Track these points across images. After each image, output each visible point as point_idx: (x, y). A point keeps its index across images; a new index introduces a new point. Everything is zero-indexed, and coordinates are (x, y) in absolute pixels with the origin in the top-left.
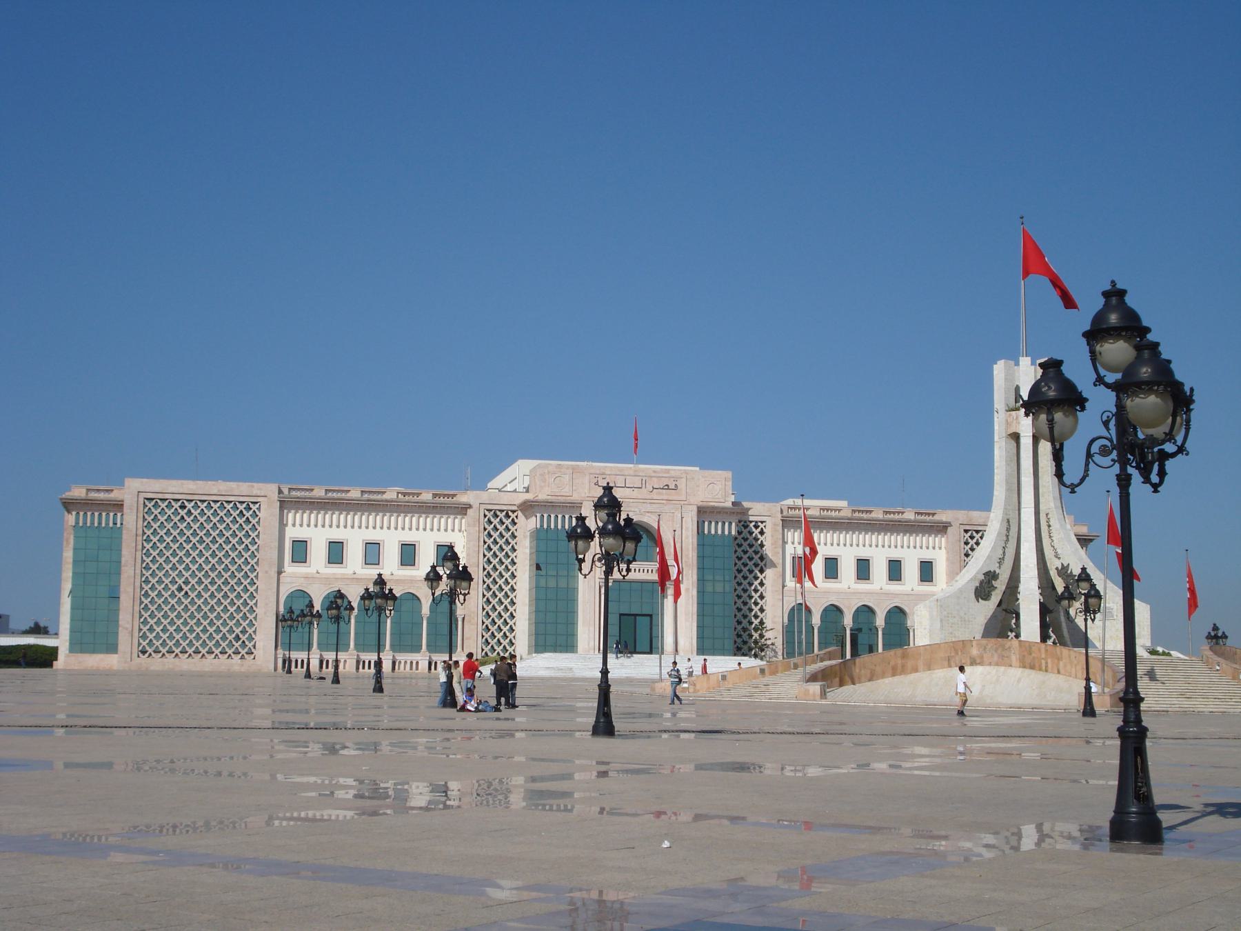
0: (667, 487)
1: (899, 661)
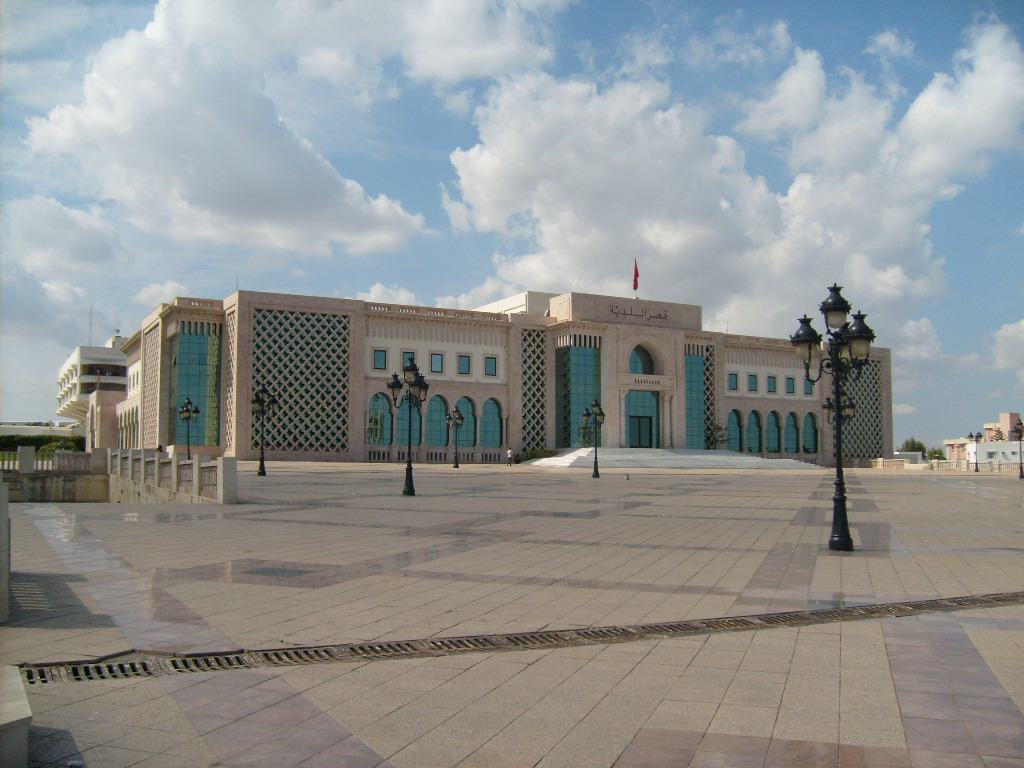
0: (659, 316)
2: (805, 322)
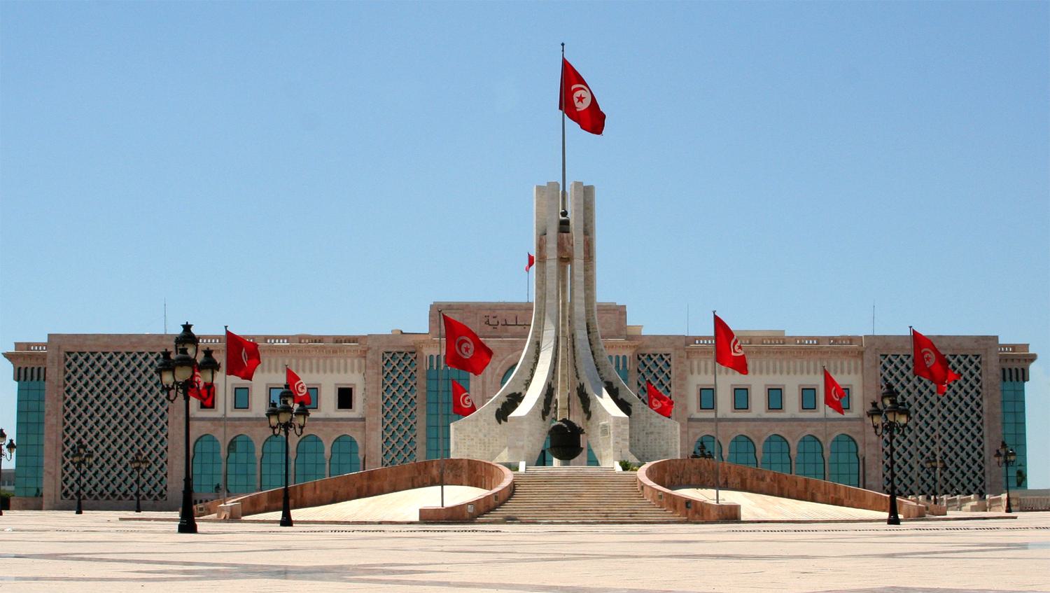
1: (365, 483)
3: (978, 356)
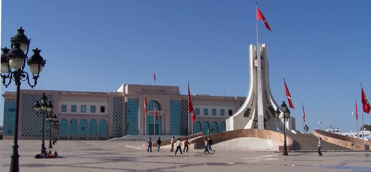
0: (162, 91)
2: (284, 102)
3: (53, 96)
